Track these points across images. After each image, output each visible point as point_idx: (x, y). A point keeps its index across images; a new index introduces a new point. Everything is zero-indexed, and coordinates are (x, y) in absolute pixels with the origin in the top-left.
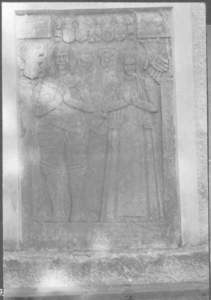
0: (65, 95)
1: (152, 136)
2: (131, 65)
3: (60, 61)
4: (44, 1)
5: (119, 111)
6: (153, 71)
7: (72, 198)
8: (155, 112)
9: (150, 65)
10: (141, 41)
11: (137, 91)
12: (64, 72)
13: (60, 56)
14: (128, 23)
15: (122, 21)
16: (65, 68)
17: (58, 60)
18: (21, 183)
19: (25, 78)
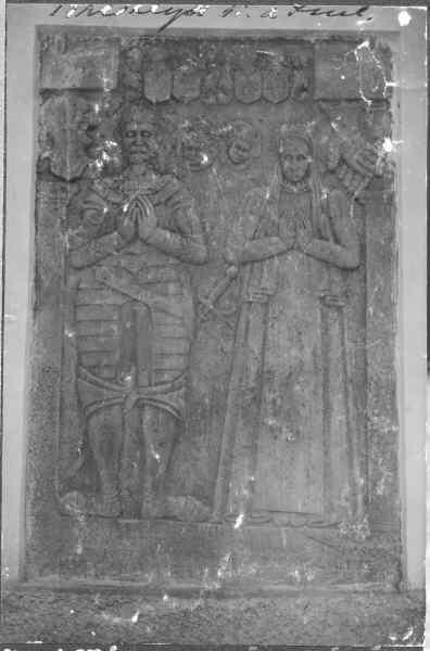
0: (142, 218)
1: (232, 439)
2: (298, 159)
3: (134, 143)
4: (428, 279)
5: (256, 265)
6: (350, 176)
7: (267, 354)
8: (352, 270)
9: (343, 161)
10: (324, 105)
11: (311, 219)
12: (143, 168)
13: (135, 133)
14: (296, 64)
15: (282, 59)
16: (145, 161)
17: (131, 140)
18: (388, 258)
19: (51, 178)
